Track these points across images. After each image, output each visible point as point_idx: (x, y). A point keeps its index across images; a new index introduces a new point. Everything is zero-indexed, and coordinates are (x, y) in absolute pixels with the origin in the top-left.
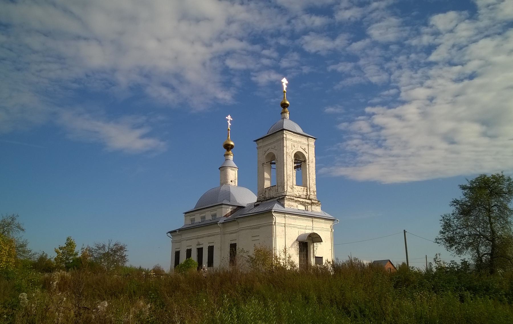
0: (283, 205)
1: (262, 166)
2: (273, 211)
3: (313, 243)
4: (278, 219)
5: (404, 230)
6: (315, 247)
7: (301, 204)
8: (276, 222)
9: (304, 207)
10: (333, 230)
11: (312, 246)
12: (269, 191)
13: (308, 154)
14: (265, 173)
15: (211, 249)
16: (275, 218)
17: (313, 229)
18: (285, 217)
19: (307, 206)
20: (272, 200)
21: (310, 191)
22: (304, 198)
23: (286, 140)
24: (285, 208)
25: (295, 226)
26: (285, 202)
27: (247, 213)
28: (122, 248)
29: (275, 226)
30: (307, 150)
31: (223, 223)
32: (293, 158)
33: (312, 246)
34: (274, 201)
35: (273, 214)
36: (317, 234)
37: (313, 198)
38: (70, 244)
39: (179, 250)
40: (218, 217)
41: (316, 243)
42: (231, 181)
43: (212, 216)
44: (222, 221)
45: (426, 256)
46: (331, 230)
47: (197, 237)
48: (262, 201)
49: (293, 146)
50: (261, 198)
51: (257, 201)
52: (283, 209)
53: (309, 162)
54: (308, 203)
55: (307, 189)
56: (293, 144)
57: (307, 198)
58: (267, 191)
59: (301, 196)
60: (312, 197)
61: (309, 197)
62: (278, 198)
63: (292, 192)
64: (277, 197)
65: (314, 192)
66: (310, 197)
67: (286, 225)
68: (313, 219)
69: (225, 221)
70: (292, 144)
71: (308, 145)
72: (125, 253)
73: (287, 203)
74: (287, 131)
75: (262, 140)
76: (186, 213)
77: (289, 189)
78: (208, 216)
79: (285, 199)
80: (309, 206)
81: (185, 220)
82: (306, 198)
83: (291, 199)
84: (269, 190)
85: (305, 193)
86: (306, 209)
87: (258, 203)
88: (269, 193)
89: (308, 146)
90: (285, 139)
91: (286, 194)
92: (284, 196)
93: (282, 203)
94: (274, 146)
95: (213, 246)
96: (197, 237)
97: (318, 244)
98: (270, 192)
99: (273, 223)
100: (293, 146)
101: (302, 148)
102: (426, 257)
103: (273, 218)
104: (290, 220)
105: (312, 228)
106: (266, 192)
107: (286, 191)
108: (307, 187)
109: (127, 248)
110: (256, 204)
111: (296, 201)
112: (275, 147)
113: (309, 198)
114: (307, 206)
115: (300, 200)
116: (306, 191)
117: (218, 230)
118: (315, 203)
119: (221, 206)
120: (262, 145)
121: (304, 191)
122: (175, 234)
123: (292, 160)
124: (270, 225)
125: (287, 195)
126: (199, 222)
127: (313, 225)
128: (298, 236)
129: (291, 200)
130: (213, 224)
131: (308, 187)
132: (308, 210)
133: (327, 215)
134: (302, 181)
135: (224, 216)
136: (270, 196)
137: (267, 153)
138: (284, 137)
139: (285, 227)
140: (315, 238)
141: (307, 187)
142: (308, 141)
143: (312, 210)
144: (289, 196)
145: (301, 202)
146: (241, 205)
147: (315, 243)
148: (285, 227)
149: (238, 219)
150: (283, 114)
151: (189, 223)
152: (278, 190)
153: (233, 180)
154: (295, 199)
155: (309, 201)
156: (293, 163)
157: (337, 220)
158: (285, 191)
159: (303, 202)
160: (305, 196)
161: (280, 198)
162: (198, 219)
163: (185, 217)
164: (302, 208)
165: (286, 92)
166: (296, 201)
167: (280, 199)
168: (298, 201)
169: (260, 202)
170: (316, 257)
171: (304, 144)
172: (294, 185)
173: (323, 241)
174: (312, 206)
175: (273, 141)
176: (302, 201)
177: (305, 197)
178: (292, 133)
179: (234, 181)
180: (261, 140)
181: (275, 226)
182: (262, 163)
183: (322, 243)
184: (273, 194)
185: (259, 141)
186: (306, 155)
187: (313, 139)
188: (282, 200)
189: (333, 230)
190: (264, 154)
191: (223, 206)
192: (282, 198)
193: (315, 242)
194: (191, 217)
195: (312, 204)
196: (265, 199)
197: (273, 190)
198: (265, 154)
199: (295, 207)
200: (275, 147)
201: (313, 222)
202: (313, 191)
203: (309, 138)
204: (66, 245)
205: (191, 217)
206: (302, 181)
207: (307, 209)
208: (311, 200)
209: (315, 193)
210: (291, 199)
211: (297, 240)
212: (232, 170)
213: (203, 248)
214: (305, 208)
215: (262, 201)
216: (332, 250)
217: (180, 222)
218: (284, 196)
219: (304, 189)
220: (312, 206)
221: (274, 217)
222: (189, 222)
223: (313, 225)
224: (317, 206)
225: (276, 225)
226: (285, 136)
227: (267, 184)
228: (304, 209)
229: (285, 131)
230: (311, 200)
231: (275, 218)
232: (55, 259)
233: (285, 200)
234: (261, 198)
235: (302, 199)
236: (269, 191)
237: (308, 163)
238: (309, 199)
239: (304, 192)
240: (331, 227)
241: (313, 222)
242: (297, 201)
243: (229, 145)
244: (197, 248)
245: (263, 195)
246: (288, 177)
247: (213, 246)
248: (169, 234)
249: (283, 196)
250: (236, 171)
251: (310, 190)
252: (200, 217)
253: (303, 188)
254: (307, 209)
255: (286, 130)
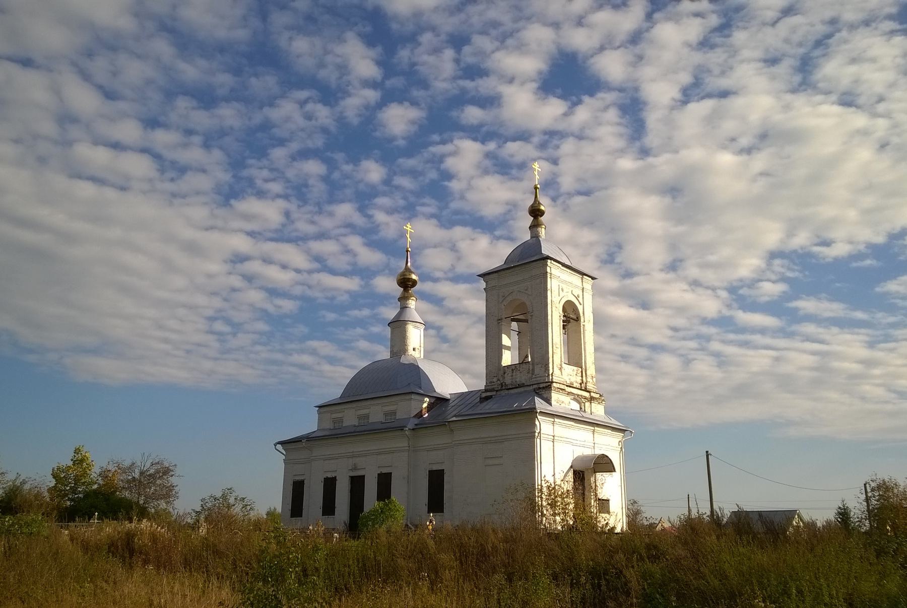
0: (548, 401)
1: (496, 323)
2: (538, 411)
3: (595, 472)
4: (544, 426)
5: (707, 452)
6: (599, 481)
7: (574, 399)
8: (542, 432)
9: (579, 406)
10: (623, 450)
11: (592, 479)
12: (513, 373)
13: (582, 306)
14: (503, 335)
15: (385, 482)
16: (540, 424)
17: (594, 447)
18: (553, 423)
19: (583, 404)
20: (522, 389)
21: (586, 376)
22: (578, 387)
23: (551, 278)
24: (551, 406)
25: (568, 440)
26: (553, 394)
27: (470, 413)
28: (167, 471)
29: (538, 440)
30: (580, 299)
31: (413, 429)
32: (561, 312)
33: (594, 478)
34: (526, 391)
35: (539, 417)
36: (607, 456)
37: (592, 388)
38: (80, 461)
39: (303, 479)
40: (400, 417)
41: (601, 473)
42: (414, 349)
43: (386, 414)
44: (410, 426)
45: (688, 495)
46: (620, 449)
47: (351, 454)
48: (497, 391)
49: (560, 289)
50: (495, 385)
51: (486, 391)
52: (549, 408)
53: (584, 321)
54: (585, 398)
55: (582, 372)
56: (560, 286)
57: (583, 388)
58: (509, 371)
59: (573, 384)
60: (590, 386)
61: (586, 386)
62: (536, 386)
63: (561, 376)
64: (532, 385)
65: (592, 377)
66: (587, 387)
67: (555, 437)
68: (596, 428)
69: (416, 425)
70: (559, 285)
71: (583, 290)
72: (173, 480)
73: (555, 396)
74: (552, 261)
75: (497, 274)
76: (320, 407)
77: (557, 372)
78: (376, 413)
79: (552, 388)
80: (586, 403)
81: (319, 419)
82: (581, 387)
83: (562, 389)
84: (512, 370)
85: (579, 379)
86: (581, 408)
87: (489, 394)
88: (512, 376)
89: (583, 292)
90: (549, 276)
91: (552, 378)
92: (549, 384)
93: (545, 396)
94: (526, 288)
95: (391, 473)
96: (351, 454)
97: (606, 475)
98: (514, 374)
99: (537, 434)
100: (560, 289)
101: (573, 295)
102: (688, 498)
103: (535, 425)
104: (563, 429)
105: (593, 445)
106: (504, 373)
107: (552, 373)
108: (582, 368)
109: (178, 471)
110: (484, 395)
111: (569, 393)
112: (526, 290)
113: (586, 388)
114: (584, 403)
115: (575, 393)
116: (580, 375)
117: (402, 443)
118: (596, 398)
119: (408, 397)
120: (496, 285)
121: (578, 375)
122: (293, 447)
123: (560, 316)
124: (530, 437)
125: (554, 381)
126: (355, 426)
127: (594, 440)
128: (572, 459)
129: (561, 391)
130: (392, 427)
131: (584, 367)
132: (585, 410)
133: (614, 422)
134: (575, 358)
135: (414, 417)
136: (516, 382)
137: (509, 299)
138: (547, 272)
139: (553, 442)
140: (603, 464)
141: (582, 368)
142: (582, 282)
143: (592, 411)
144: (558, 384)
145: (576, 396)
146: (443, 396)
147: (598, 473)
148: (553, 442)
149: (450, 423)
150: (535, 229)
151: (328, 427)
152: (533, 370)
153: (417, 346)
154: (567, 390)
155: (586, 394)
156: (562, 320)
157: (631, 432)
158: (550, 373)
159: (578, 395)
160: (579, 385)
161: (541, 386)
162: (350, 418)
163: (319, 414)
164: (576, 406)
165: (538, 188)
166: (569, 393)
167: (540, 388)
168: (572, 393)
169: (494, 393)
170: (599, 499)
171: (577, 287)
172: (563, 363)
173: (616, 470)
174: (591, 403)
175: (522, 279)
176: (577, 395)
177: (578, 386)
178: (560, 266)
179: (418, 349)
180: (495, 275)
181: (538, 440)
182: (496, 318)
183: (613, 473)
184: (521, 378)
185: (492, 276)
186: (580, 308)
187: (590, 279)
188: (546, 391)
189: (623, 450)
190: (501, 301)
191: (413, 396)
192: (546, 387)
193: (599, 472)
194: (334, 416)
195: (592, 399)
196: (504, 388)
197: (521, 370)
198: (503, 301)
199: (567, 404)
200: (526, 290)
201: (593, 434)
202: (591, 375)
203: (585, 277)
204: (70, 463)
205: (334, 416)
206: (575, 358)
207: (583, 408)
208: (590, 392)
209: (594, 379)
210: (561, 389)
211: (571, 467)
212: (415, 327)
213: (364, 476)
214: (580, 406)
215: (497, 391)
216: (621, 486)
217: (309, 424)
218: (549, 384)
219: (577, 370)
220: (591, 404)
221: (537, 423)
222: (328, 425)
223: (594, 440)
224: (599, 403)
225: (540, 439)
226: (548, 269)
227: (508, 359)
228: (579, 409)
229: (549, 261)
230: (590, 392)
231: (540, 424)
232: (50, 490)
233: (552, 390)
234: (495, 385)
235: (577, 390)
236: (513, 373)
237: (584, 324)
238: (586, 390)
239: (577, 377)
240: (620, 443)
241: (593, 434)
242: (570, 393)
243: (410, 280)
244: (350, 477)
245: (498, 380)
246: (554, 347)
247: (391, 473)
248: (279, 447)
249: (546, 382)
250: (422, 330)
251: (586, 374)
252: (357, 416)
253: (576, 368)
254: (583, 410)
255: (551, 259)
